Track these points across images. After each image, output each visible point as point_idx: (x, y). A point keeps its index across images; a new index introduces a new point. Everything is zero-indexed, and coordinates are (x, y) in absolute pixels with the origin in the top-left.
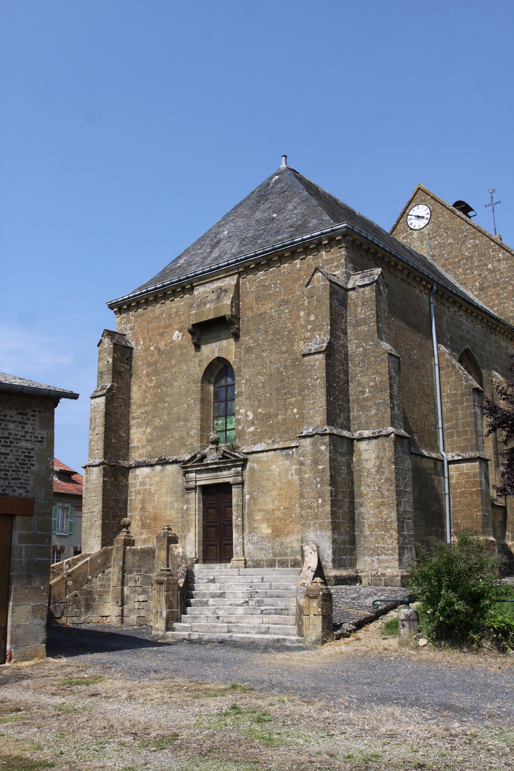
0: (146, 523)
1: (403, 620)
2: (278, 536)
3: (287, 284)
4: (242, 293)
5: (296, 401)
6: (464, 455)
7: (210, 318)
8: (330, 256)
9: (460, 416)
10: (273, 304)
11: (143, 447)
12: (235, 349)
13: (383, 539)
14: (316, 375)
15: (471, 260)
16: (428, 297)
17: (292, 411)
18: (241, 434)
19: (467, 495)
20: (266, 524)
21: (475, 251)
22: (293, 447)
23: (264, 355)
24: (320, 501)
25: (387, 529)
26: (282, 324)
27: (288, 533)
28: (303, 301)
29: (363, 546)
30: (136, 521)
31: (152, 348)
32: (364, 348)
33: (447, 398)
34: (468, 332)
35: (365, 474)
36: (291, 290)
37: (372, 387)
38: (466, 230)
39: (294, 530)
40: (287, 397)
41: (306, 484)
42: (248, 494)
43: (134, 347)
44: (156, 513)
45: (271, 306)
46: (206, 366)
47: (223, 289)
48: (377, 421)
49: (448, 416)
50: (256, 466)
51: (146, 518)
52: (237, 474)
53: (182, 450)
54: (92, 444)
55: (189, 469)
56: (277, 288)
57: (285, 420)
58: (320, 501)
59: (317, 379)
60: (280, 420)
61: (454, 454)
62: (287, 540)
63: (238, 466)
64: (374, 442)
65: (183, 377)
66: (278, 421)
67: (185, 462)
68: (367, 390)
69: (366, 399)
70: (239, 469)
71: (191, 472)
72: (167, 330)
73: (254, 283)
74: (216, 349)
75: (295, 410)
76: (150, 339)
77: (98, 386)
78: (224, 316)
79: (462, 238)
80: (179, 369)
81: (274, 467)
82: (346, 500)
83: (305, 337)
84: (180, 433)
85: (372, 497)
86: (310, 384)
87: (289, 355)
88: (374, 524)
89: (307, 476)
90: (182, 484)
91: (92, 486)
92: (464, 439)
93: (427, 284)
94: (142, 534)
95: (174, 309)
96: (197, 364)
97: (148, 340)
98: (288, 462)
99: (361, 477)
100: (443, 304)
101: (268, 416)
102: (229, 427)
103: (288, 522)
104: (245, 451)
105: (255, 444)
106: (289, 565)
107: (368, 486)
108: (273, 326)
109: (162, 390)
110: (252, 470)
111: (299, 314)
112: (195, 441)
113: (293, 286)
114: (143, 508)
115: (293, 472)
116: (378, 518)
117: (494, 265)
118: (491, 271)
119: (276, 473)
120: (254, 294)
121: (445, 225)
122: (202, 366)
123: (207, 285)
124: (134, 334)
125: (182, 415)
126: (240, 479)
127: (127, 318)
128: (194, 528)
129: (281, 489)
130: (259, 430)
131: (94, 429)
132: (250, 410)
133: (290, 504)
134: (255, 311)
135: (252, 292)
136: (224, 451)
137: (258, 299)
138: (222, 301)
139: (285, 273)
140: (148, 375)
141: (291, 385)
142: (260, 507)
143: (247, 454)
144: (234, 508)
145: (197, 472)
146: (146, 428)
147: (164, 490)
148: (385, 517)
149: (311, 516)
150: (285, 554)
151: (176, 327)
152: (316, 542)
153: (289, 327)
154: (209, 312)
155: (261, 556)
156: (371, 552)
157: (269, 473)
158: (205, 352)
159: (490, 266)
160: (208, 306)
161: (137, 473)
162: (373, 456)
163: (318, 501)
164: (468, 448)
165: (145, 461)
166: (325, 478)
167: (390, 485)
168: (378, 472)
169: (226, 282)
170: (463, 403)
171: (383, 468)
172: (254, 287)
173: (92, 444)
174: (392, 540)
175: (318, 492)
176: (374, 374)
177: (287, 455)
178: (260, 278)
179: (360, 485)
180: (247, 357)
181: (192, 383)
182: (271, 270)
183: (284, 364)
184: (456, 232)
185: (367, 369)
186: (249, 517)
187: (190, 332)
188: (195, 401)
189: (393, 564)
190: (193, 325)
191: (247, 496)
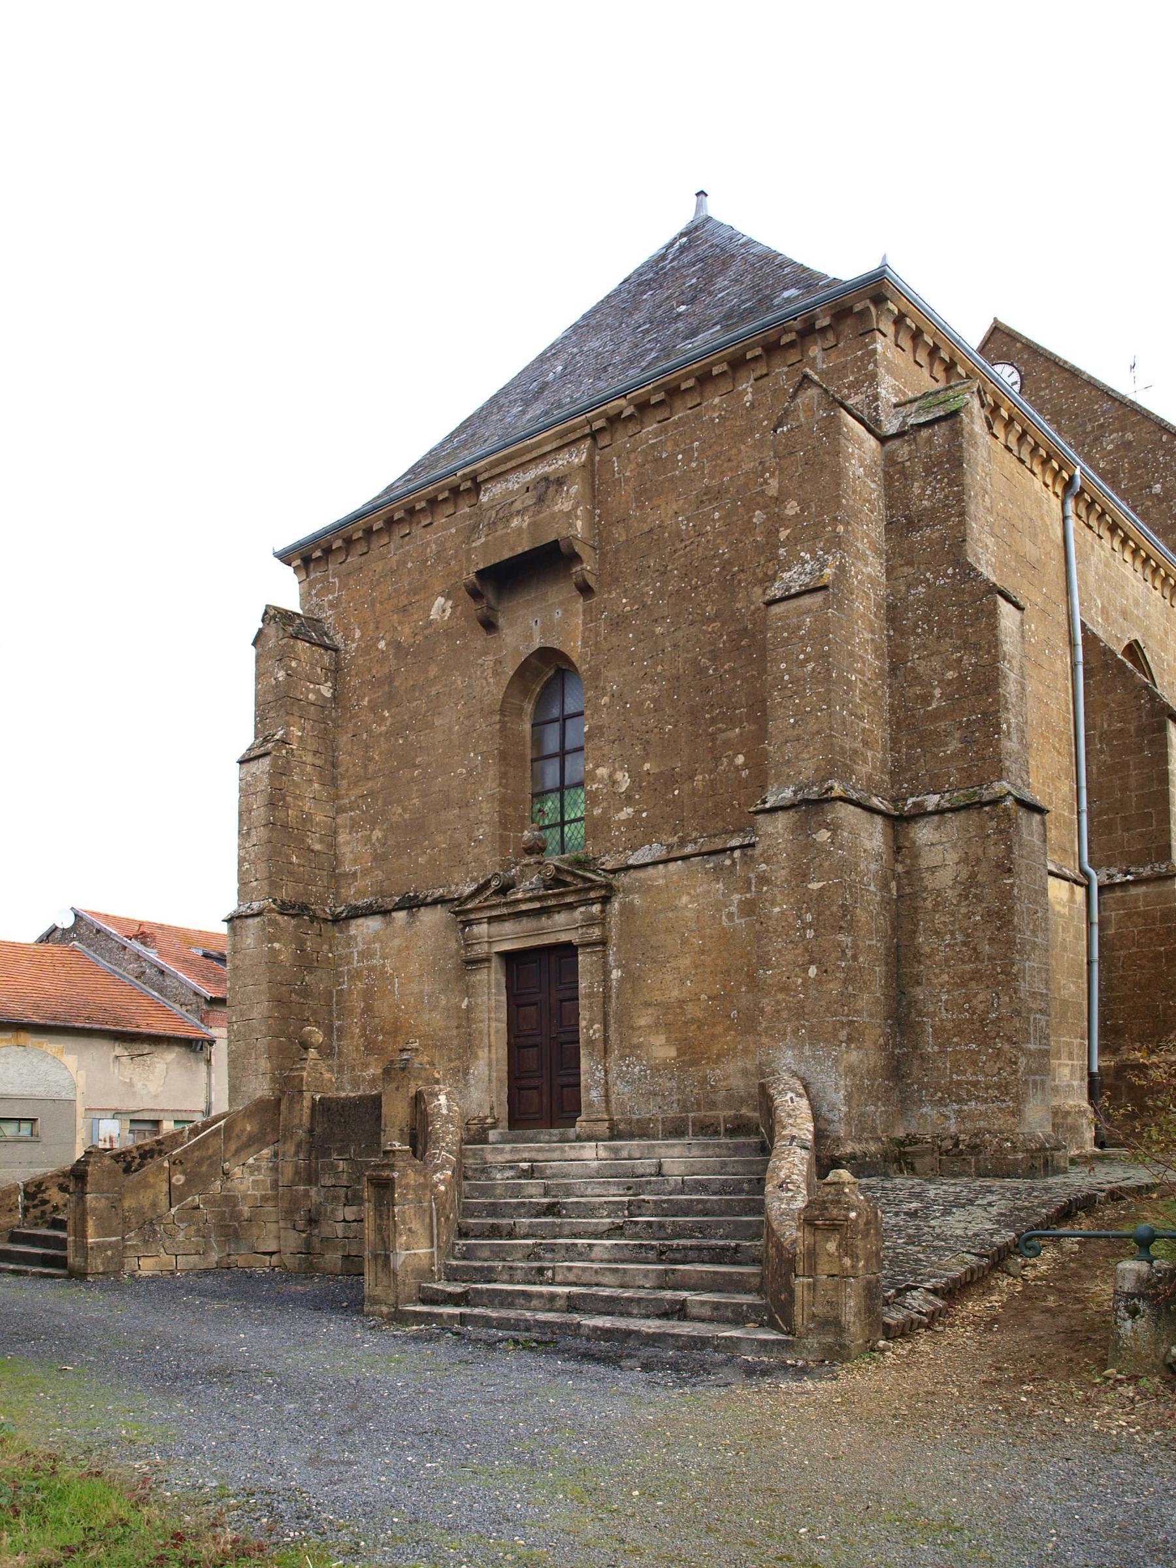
0: (375, 1042)
1: (1131, 1296)
2: (694, 1063)
3: (719, 449)
4: (601, 484)
5: (741, 734)
6: (1141, 870)
7: (520, 551)
8: (835, 360)
9: (1133, 782)
10: (681, 502)
11: (366, 872)
12: (585, 624)
13: (974, 1063)
14: (803, 652)
15: (1113, 477)
16: (1059, 502)
17: (731, 760)
18: (596, 828)
19: (1144, 962)
20: (663, 1037)
21: (1122, 458)
22: (733, 849)
23: (659, 630)
24: (813, 971)
25: (987, 1036)
26: (705, 549)
27: (719, 1056)
28: (761, 485)
29: (919, 1081)
30: (352, 1038)
31: (382, 645)
32: (929, 586)
33: (1101, 741)
34: (1137, 604)
35: (929, 904)
36: (729, 460)
37: (950, 683)
38: (1104, 413)
39: (736, 1048)
40: (719, 729)
41: (775, 931)
42: (618, 967)
43: (342, 646)
44: (396, 1019)
45: (675, 507)
46: (511, 673)
47: (552, 478)
48: (963, 769)
49: (1100, 783)
50: (637, 900)
51: (375, 1031)
52: (590, 922)
53: (456, 875)
54: (244, 869)
55: (472, 916)
56: (691, 461)
57: (712, 784)
58: (813, 971)
59: (807, 660)
60: (700, 787)
61: (1113, 871)
62: (715, 1073)
63: (592, 902)
64: (954, 822)
65: (456, 705)
66: (694, 789)
67: (462, 900)
68: (937, 692)
69: (935, 716)
70: (596, 908)
71: (478, 922)
72: (417, 597)
73: (632, 456)
74: (536, 629)
75: (740, 759)
76: (378, 622)
77: (256, 738)
78: (556, 542)
79: (1093, 431)
80: (446, 686)
81: (685, 899)
82: (877, 969)
83: (766, 574)
84: (451, 837)
85: (947, 960)
86: (786, 677)
87: (723, 626)
88: (950, 1025)
89: (777, 910)
90: (458, 951)
91: (247, 962)
92: (1142, 835)
93: (1061, 468)
94: (366, 1066)
95: (434, 546)
96: (490, 671)
97: (372, 626)
98: (720, 886)
99: (916, 912)
100: (1090, 527)
101: (669, 779)
102: (570, 815)
103: (719, 1029)
104: (608, 866)
105: (634, 849)
106: (722, 1129)
107: (937, 933)
108: (680, 557)
109: (406, 738)
110: (628, 911)
111: (751, 518)
112: (488, 852)
113: (734, 451)
114: (368, 1009)
115: (733, 909)
116: (962, 1010)
117: (1168, 485)
118: (1159, 499)
119: (688, 914)
120: (632, 483)
121: (1054, 405)
122: (503, 672)
123: (512, 477)
124: (339, 617)
125: (455, 795)
126: (596, 932)
127: (322, 582)
128: (486, 1050)
129: (703, 952)
130: (644, 815)
131: (248, 833)
132: (622, 768)
133: (724, 987)
134: (635, 524)
135: (627, 480)
136: (557, 868)
137: (643, 494)
138: (548, 507)
139: (712, 420)
140: (373, 708)
141: (730, 697)
142: (647, 998)
143: (614, 871)
144: (582, 1002)
145: (491, 920)
146: (372, 831)
147: (414, 967)
148: (982, 1007)
149: (789, 1009)
150: (713, 1105)
151: (438, 589)
152: (801, 1074)
153: (724, 554)
154: (518, 536)
155: (649, 1110)
156: (940, 1094)
157: (670, 915)
158: (508, 640)
159: (1157, 488)
160: (515, 522)
161: (352, 933)
162: (952, 857)
163: (806, 971)
164: (1150, 855)
165: (371, 904)
166: (828, 912)
167: (998, 929)
168: (964, 896)
169: (560, 462)
170: (1142, 750)
171: (978, 885)
172: (633, 466)
173: (244, 869)
174: (998, 1065)
175: (806, 949)
176: (957, 649)
177: (719, 869)
178: (647, 442)
179: (915, 932)
180: (614, 640)
181: (478, 715)
182: (676, 417)
183: (709, 648)
184: (1079, 420)
185: (939, 638)
186: (620, 1021)
187: (475, 594)
188: (485, 759)
189: (1001, 1122)
190: (480, 574)
191: (614, 972)
